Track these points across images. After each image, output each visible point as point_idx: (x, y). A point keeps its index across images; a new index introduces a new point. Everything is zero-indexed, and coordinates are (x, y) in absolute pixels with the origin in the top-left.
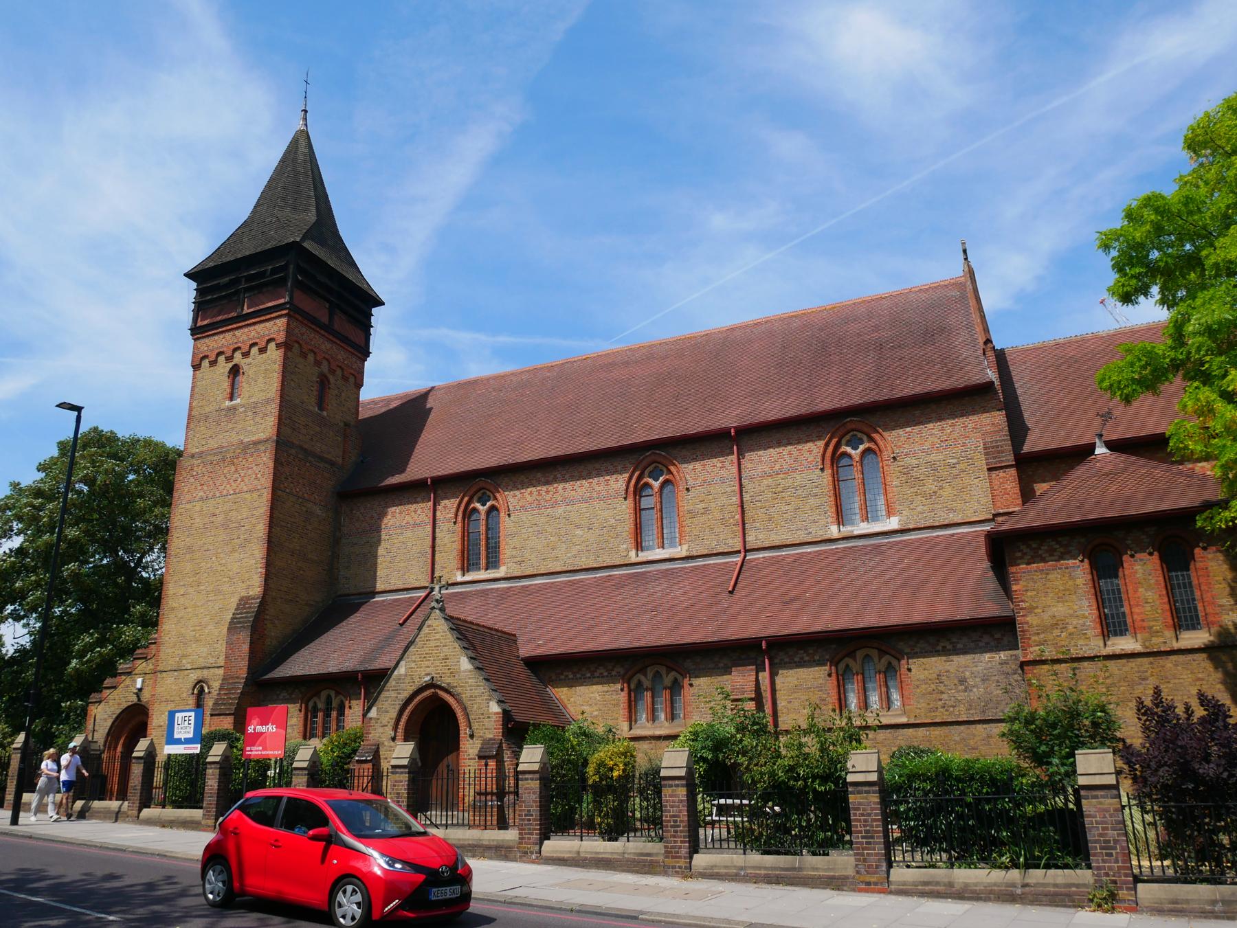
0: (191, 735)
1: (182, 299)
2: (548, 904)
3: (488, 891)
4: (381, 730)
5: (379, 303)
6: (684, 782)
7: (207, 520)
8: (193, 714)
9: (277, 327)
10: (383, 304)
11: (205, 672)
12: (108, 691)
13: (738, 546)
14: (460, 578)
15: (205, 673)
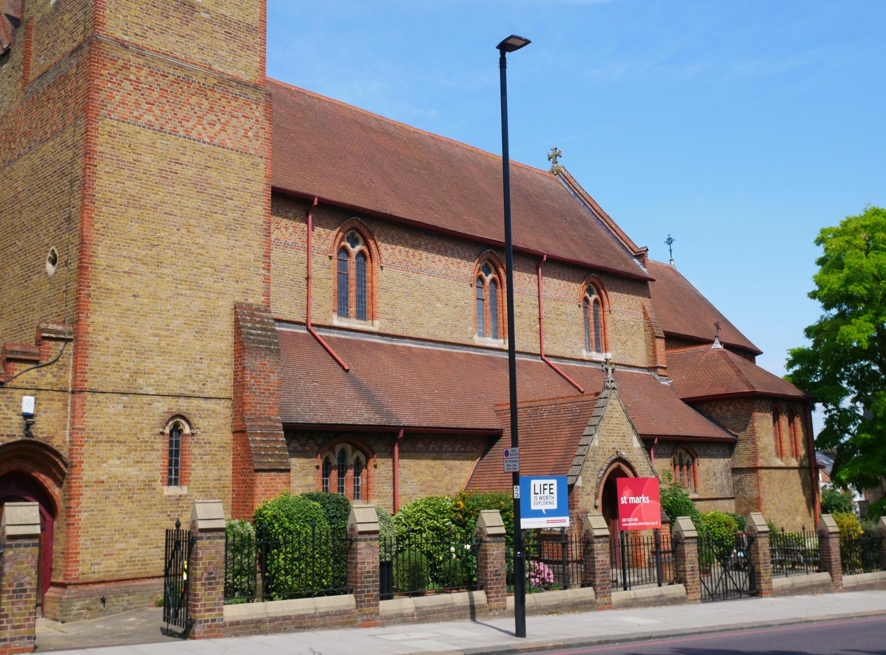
0: (554, 506)
2: (697, 631)
4: (586, 498)
6: (608, 540)
7: (164, 164)
8: (554, 482)
11: (183, 402)
15: (183, 405)
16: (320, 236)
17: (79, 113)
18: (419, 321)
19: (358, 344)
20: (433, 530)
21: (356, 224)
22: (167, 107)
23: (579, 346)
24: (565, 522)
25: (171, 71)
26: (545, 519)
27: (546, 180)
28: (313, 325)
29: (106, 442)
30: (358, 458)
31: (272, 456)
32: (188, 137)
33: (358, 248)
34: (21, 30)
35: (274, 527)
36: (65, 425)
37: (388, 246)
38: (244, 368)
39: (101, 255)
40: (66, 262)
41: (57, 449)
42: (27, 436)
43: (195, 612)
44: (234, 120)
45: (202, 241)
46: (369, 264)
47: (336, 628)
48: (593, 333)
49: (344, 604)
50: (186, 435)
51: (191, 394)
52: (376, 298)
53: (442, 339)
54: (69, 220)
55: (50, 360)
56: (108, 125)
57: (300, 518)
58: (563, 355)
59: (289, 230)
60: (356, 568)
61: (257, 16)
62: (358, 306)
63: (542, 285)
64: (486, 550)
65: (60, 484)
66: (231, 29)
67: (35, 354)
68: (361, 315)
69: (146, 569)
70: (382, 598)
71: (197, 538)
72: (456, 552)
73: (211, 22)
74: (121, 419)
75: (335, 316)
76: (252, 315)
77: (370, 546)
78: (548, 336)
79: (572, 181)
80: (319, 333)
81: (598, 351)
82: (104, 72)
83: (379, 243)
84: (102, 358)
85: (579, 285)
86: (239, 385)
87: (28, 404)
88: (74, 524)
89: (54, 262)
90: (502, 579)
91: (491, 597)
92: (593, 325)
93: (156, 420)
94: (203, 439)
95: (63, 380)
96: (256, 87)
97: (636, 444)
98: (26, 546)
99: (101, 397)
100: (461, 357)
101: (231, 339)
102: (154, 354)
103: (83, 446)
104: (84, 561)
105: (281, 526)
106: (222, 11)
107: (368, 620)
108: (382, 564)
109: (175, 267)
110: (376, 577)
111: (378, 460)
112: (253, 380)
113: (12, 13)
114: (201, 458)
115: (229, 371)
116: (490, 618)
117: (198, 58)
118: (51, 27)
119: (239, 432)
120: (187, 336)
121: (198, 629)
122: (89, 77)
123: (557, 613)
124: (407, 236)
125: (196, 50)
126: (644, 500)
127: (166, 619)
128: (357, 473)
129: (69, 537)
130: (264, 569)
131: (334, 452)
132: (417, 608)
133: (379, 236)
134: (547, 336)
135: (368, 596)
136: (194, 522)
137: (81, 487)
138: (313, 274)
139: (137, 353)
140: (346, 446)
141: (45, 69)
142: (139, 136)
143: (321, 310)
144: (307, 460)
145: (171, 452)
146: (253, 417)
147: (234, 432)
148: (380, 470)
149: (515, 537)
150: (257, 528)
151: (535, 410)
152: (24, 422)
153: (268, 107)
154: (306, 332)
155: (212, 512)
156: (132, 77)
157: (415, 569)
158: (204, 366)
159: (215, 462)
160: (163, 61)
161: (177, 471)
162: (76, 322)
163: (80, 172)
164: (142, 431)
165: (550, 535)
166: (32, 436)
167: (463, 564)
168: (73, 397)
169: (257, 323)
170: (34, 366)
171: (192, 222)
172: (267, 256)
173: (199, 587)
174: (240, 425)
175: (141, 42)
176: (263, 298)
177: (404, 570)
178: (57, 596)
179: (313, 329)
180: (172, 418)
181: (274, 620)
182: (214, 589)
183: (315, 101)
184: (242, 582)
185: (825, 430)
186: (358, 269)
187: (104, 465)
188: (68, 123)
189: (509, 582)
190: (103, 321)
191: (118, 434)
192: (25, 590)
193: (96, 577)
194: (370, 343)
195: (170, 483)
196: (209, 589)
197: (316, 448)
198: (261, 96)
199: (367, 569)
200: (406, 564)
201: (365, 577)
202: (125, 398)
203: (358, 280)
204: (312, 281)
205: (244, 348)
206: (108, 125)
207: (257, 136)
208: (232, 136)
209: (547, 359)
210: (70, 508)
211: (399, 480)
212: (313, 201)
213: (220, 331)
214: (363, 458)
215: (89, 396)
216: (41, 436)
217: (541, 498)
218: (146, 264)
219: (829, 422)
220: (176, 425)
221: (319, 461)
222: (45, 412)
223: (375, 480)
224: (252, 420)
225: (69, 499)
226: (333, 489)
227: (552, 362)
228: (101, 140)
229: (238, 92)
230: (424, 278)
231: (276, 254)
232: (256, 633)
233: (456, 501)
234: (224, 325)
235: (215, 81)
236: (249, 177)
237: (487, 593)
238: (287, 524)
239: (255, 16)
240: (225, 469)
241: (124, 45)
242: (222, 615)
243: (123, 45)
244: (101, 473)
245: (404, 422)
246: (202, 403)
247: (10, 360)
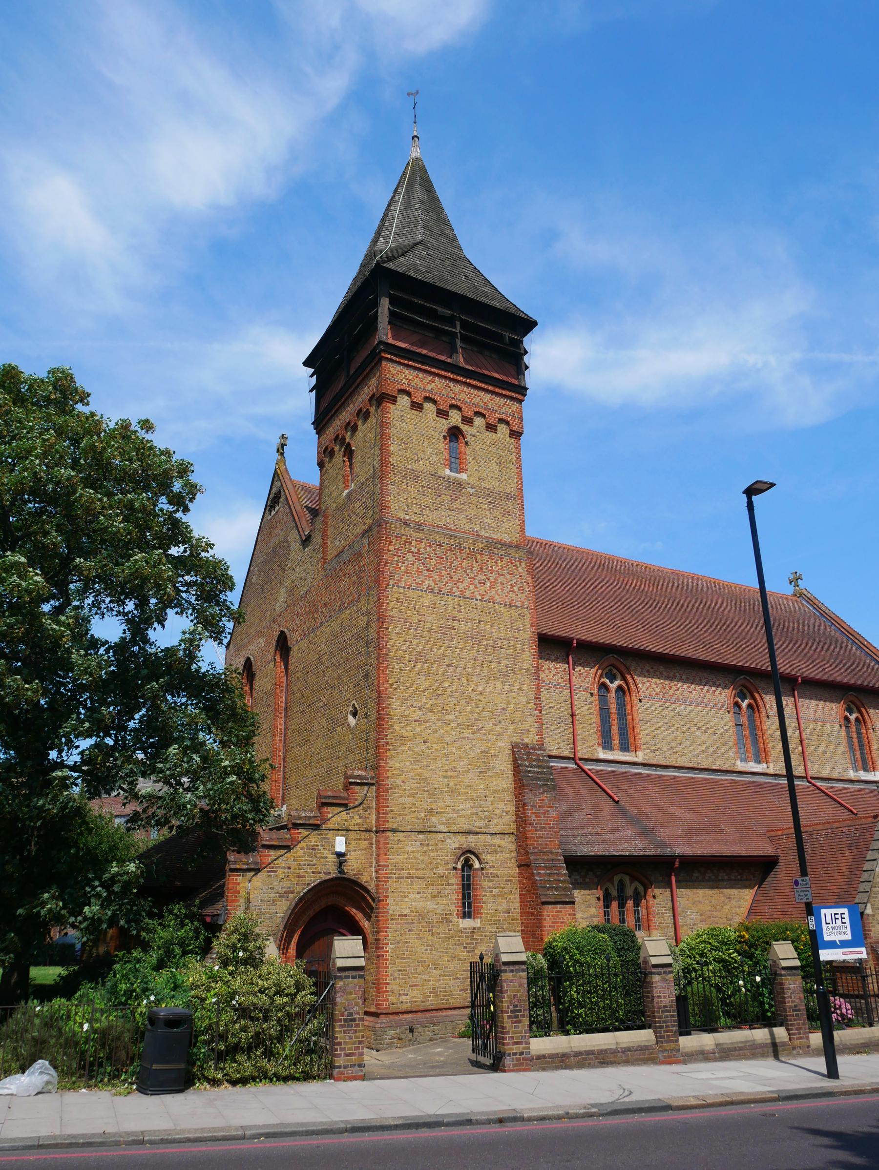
0: (849, 937)
7: (444, 622)
8: (845, 911)
10: (534, 324)
11: (471, 838)
12: (273, 854)
15: (472, 841)
16: (580, 674)
17: (372, 584)
18: (680, 750)
19: (625, 775)
20: (719, 962)
22: (444, 572)
23: (845, 766)
24: (861, 953)
25: (446, 541)
26: (840, 951)
27: (790, 603)
28: (580, 759)
29: (407, 878)
30: (636, 889)
31: (556, 889)
33: (617, 683)
34: (320, 519)
35: (565, 960)
36: (371, 863)
37: (645, 680)
38: (525, 804)
39: (396, 707)
40: (366, 714)
41: (366, 884)
42: (340, 873)
43: (504, 1044)
44: (501, 577)
45: (480, 688)
46: (628, 698)
47: (639, 1065)
48: (858, 753)
49: (644, 1039)
50: (477, 870)
51: (479, 830)
52: (637, 729)
53: (705, 767)
54: (367, 677)
55: (357, 803)
56: (395, 592)
57: (590, 950)
58: (830, 776)
59: (554, 671)
60: (652, 1001)
61: (515, 486)
62: (621, 739)
63: (799, 707)
64: (782, 984)
65: (369, 918)
66: (493, 499)
67: (344, 798)
68: (625, 747)
69: (447, 999)
70: (681, 1035)
71: (501, 971)
72: (745, 986)
73: (476, 495)
74: (419, 856)
75: (600, 749)
76: (528, 754)
77: (664, 980)
78: (811, 758)
79: (816, 602)
80: (587, 767)
81: (866, 770)
82: (391, 548)
83: (764, 696)
84: (400, 799)
85: (837, 705)
86: (521, 820)
87: (340, 844)
88: (382, 956)
89: (355, 714)
90: (802, 1015)
91: (793, 1034)
93: (449, 856)
94: (492, 873)
95: (368, 821)
96: (518, 547)
98: (354, 977)
99: (401, 836)
100: (726, 783)
101: (511, 777)
102: (444, 794)
103: (387, 881)
104: (393, 991)
105: (571, 958)
106: (485, 485)
107: (670, 1057)
108: (678, 998)
109: (457, 713)
110: (673, 1011)
111: (655, 890)
112: (533, 816)
113: (309, 504)
114: (491, 892)
115: (511, 807)
116: (794, 1057)
117: (467, 527)
118: (345, 514)
119: (524, 866)
120: (472, 776)
121: (508, 1061)
122: (379, 553)
123: (865, 1052)
124: (662, 668)
125: (465, 521)
127: (475, 1050)
128: (637, 904)
129: (379, 968)
130: (558, 1001)
131: (613, 884)
132: (717, 1045)
133: (636, 671)
134: (810, 758)
135: (667, 1031)
136: (497, 955)
137: (387, 920)
138: (577, 710)
139: (430, 794)
140: (624, 877)
141: (341, 548)
142: (422, 600)
143: (587, 744)
144: (588, 892)
145: (463, 885)
146: (536, 851)
147: (519, 866)
148: (659, 900)
149: (812, 968)
150: (548, 960)
151: (810, 835)
152: (338, 860)
153: (530, 563)
154: (574, 766)
155: (512, 946)
156: (414, 550)
157: (706, 1003)
158: (488, 804)
159: (504, 895)
160: (438, 533)
161: (469, 904)
162: (377, 768)
163: (375, 635)
164: (437, 867)
165: (842, 967)
166: (345, 874)
167: (755, 998)
168: (377, 837)
169: (534, 761)
170: (343, 809)
171: (471, 671)
172: (538, 698)
173: (506, 1020)
174: (525, 859)
175: (419, 519)
176: (537, 737)
177: (694, 1005)
178: (371, 1025)
179: (581, 763)
180: (463, 854)
181: (578, 1054)
182: (520, 1022)
183: (564, 550)
184: (537, 1015)
186: (618, 704)
187: (406, 900)
188: (362, 593)
189: (811, 1017)
190: (399, 765)
191: (417, 870)
192: (354, 1020)
193: (403, 1007)
194: (635, 774)
195: (464, 917)
196: (516, 1022)
197: (596, 880)
198: (522, 554)
199: (664, 1004)
200: (696, 998)
201: (663, 1012)
202: (421, 836)
203: (619, 714)
204: (576, 718)
205: (523, 786)
206: (395, 592)
207: (521, 590)
208: (500, 592)
209: (813, 781)
210: (379, 940)
211: (679, 910)
212: (572, 643)
213: (500, 770)
214: (641, 889)
215: (390, 834)
216: (351, 873)
217: (833, 928)
218: (434, 712)
220: (467, 860)
221: (599, 893)
222: (354, 851)
223: (654, 911)
224: (535, 854)
225: (378, 932)
226: (615, 921)
227: (819, 784)
228: (391, 605)
229: (502, 553)
230: (682, 708)
231: (544, 693)
232: (562, 1068)
233: (739, 931)
234: (504, 764)
235: (483, 546)
236: (517, 627)
237: (788, 1030)
238: (578, 957)
239: (513, 485)
240: (513, 902)
241: (406, 523)
242: (529, 1048)
243: (405, 523)
244: (404, 907)
245: (678, 851)
246: (489, 839)
247: (324, 804)
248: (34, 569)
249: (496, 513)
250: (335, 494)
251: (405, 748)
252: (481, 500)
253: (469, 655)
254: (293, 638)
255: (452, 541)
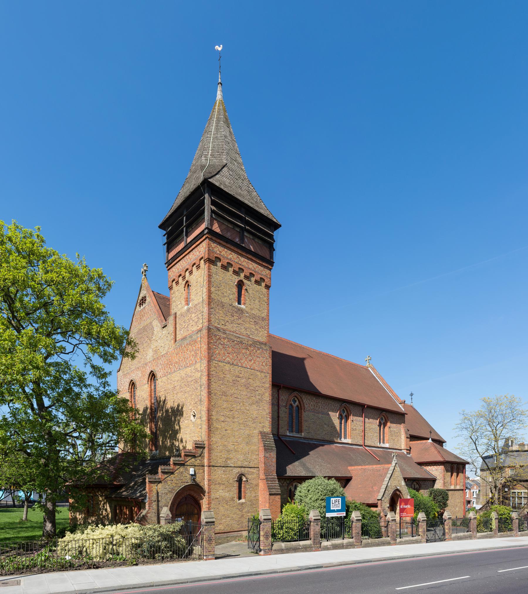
0: (340, 508)
1: (160, 237)
2: (289, 569)
3: (164, 580)
5: (446, 442)
8: (340, 499)
9: (202, 249)
10: (280, 226)
11: (243, 469)
13: (361, 443)
14: (288, 434)
21: (296, 395)
32: (242, 367)
45: (248, 408)
61: (266, 314)
74: (223, 476)
75: (288, 432)
92: (294, 418)
97: (403, 483)
99: (216, 468)
118: (186, 318)
126: (409, 506)
138: (280, 415)
156: (222, 343)
185: (311, 450)
207: (266, 365)
219: (92, 515)
230: (320, 416)
241: (218, 329)
243: (218, 329)
248: (100, 509)
249: (257, 327)
250: (180, 306)
251: (218, 433)
252: (251, 320)
253: (244, 393)
254: (159, 375)
255: (238, 340)
